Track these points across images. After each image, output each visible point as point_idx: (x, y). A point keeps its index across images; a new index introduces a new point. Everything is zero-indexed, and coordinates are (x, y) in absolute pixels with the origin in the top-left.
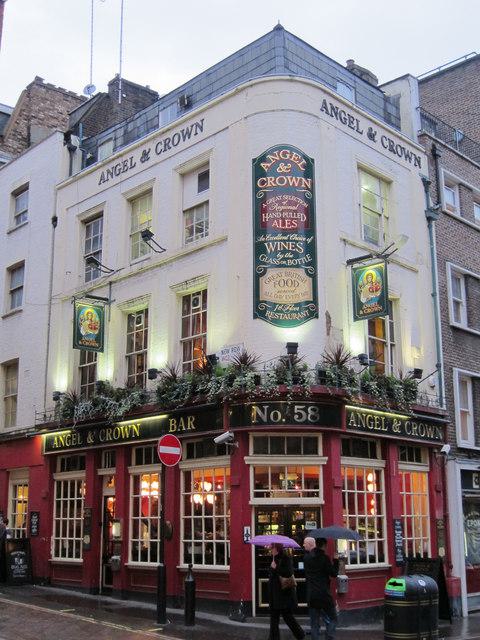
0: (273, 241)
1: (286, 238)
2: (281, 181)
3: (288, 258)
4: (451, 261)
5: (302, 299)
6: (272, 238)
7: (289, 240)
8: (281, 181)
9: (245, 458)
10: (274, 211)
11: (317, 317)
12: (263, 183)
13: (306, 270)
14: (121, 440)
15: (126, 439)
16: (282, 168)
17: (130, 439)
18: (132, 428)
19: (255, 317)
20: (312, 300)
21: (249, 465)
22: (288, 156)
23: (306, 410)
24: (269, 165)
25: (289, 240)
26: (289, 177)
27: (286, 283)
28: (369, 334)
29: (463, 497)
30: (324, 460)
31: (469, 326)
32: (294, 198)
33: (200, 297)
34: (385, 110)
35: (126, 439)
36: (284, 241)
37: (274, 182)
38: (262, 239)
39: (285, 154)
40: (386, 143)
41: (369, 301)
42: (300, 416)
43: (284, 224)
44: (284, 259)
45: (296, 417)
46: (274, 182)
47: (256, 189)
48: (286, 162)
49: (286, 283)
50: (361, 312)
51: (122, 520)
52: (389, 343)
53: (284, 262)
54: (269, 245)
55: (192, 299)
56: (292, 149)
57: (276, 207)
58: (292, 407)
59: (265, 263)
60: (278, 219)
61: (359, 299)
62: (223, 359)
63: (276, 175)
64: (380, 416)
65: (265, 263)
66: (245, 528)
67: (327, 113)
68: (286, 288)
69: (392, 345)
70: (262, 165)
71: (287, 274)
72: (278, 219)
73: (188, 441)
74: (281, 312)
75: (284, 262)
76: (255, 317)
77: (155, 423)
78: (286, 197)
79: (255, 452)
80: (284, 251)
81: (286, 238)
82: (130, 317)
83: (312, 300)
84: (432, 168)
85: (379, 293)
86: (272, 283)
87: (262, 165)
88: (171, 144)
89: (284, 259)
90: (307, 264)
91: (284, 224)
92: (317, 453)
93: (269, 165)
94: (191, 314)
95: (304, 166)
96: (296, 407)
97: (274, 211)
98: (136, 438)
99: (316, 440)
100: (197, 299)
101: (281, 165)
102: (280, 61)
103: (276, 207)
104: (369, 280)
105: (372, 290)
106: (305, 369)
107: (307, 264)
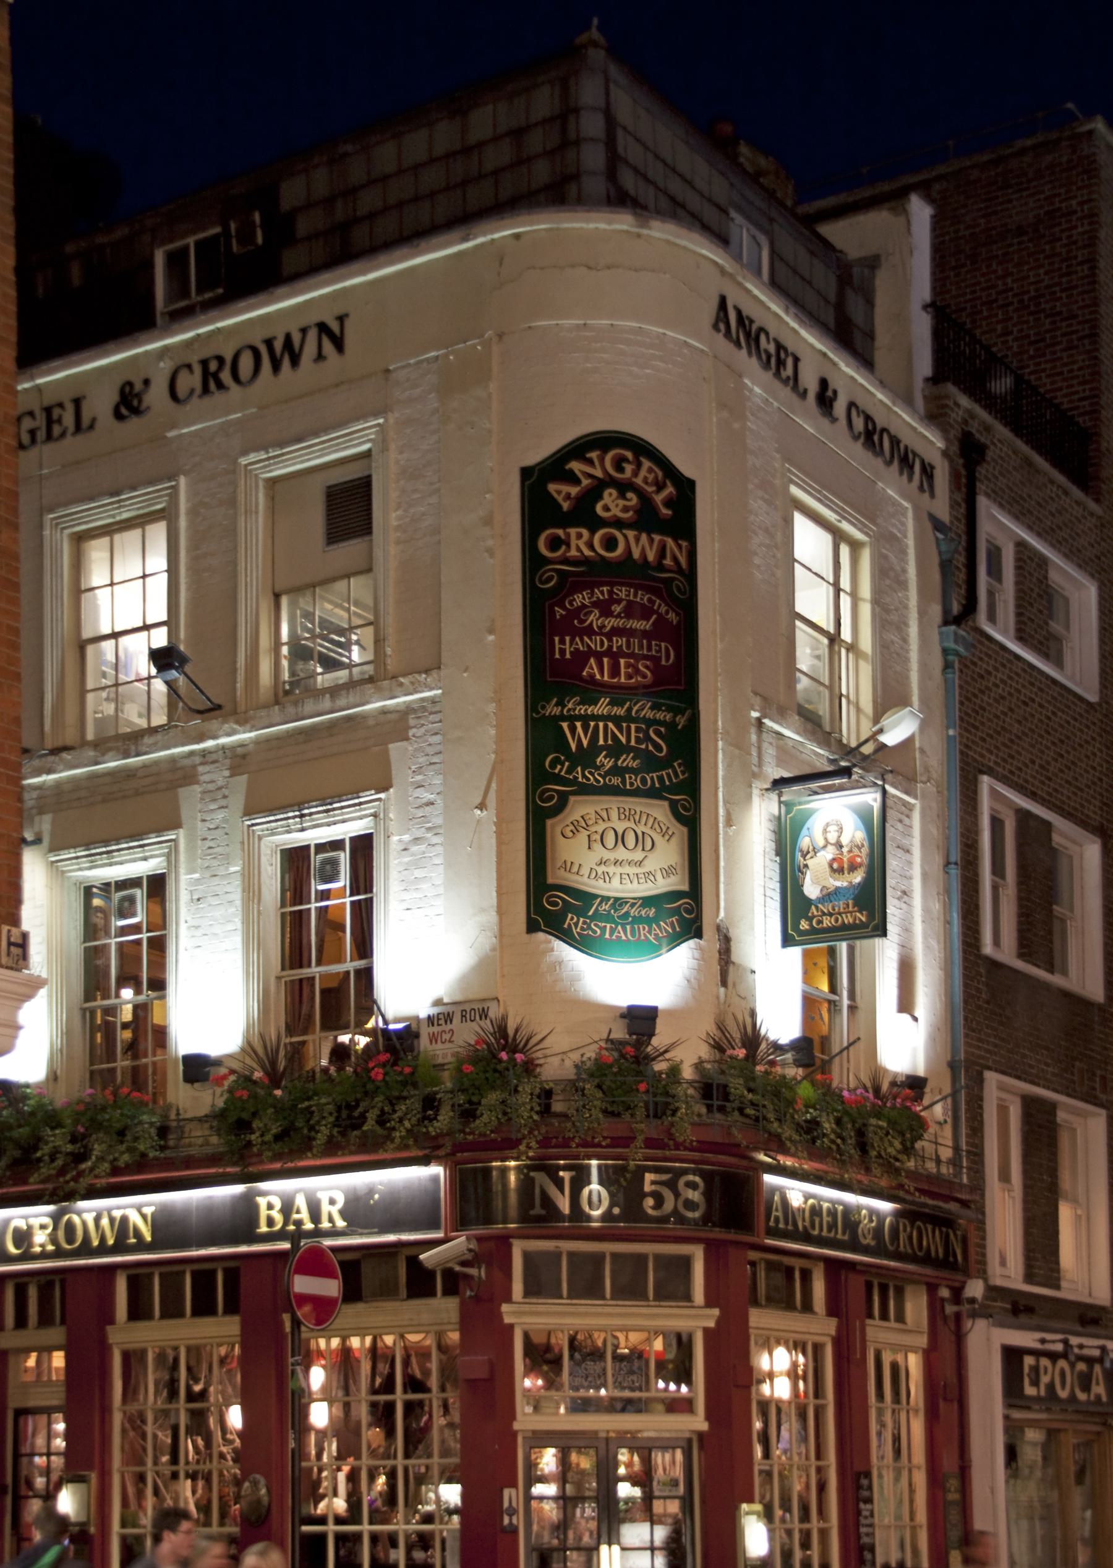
0: (585, 719)
1: (620, 711)
2: (610, 543)
3: (628, 770)
4: (991, 772)
5: (662, 885)
6: (582, 710)
7: (628, 718)
8: (610, 543)
9: (505, 1308)
10: (590, 631)
11: (699, 935)
12: (555, 543)
13: (673, 806)
14: (86, 1249)
15: (103, 1249)
16: (610, 504)
17: (120, 1247)
18: (124, 1220)
19: (532, 927)
20: (685, 887)
21: (511, 1327)
22: (629, 468)
23: (672, 1185)
24: (574, 491)
25: (628, 718)
26: (631, 534)
27: (621, 839)
28: (352, 839)
29: (1006, 1418)
30: (710, 1318)
31: (1021, 956)
32: (643, 598)
33: (344, 858)
34: (840, 306)
35: (103, 1249)
36: (617, 720)
37: (591, 546)
38: (552, 709)
39: (619, 464)
40: (859, 424)
41: (829, 896)
42: (659, 1201)
43: (615, 671)
44: (616, 771)
45: (650, 1202)
46: (591, 546)
47: (532, 562)
48: (623, 488)
49: (621, 839)
50: (804, 925)
51: (94, 1477)
52: (846, 1002)
53: (616, 781)
54: (573, 729)
55: (316, 860)
56: (642, 449)
57: (594, 619)
58: (640, 1172)
59: (559, 779)
60: (599, 656)
61: (798, 887)
62: (433, 1038)
63: (594, 523)
64: (833, 1202)
65: (559, 779)
66: (506, 1492)
67: (728, 334)
68: (621, 853)
69: (852, 1008)
70: (552, 487)
71: (625, 815)
72: (599, 656)
73: (196, 1267)
74: (608, 918)
75: (616, 781)
76: (532, 927)
77: (208, 1209)
78: (622, 593)
79: (527, 1293)
80: (616, 749)
81: (620, 711)
82: (88, 892)
83: (685, 887)
84: (959, 497)
85: (858, 878)
86: (584, 834)
87: (552, 487)
88: (226, 376)
89: (616, 771)
90: (675, 789)
91: (615, 671)
92: (688, 1297)
93: (574, 491)
94: (313, 906)
95: (668, 503)
96: (649, 1177)
97: (590, 631)
98: (141, 1246)
99: (685, 1263)
100: (334, 863)
101: (609, 496)
102: (593, 157)
103: (594, 619)
104: (832, 837)
105: (837, 868)
106: (674, 1071)
107: (675, 789)
